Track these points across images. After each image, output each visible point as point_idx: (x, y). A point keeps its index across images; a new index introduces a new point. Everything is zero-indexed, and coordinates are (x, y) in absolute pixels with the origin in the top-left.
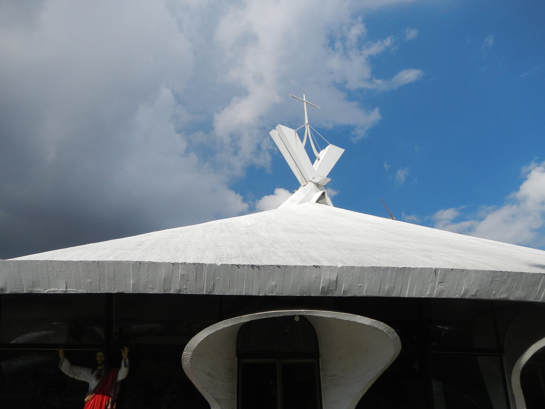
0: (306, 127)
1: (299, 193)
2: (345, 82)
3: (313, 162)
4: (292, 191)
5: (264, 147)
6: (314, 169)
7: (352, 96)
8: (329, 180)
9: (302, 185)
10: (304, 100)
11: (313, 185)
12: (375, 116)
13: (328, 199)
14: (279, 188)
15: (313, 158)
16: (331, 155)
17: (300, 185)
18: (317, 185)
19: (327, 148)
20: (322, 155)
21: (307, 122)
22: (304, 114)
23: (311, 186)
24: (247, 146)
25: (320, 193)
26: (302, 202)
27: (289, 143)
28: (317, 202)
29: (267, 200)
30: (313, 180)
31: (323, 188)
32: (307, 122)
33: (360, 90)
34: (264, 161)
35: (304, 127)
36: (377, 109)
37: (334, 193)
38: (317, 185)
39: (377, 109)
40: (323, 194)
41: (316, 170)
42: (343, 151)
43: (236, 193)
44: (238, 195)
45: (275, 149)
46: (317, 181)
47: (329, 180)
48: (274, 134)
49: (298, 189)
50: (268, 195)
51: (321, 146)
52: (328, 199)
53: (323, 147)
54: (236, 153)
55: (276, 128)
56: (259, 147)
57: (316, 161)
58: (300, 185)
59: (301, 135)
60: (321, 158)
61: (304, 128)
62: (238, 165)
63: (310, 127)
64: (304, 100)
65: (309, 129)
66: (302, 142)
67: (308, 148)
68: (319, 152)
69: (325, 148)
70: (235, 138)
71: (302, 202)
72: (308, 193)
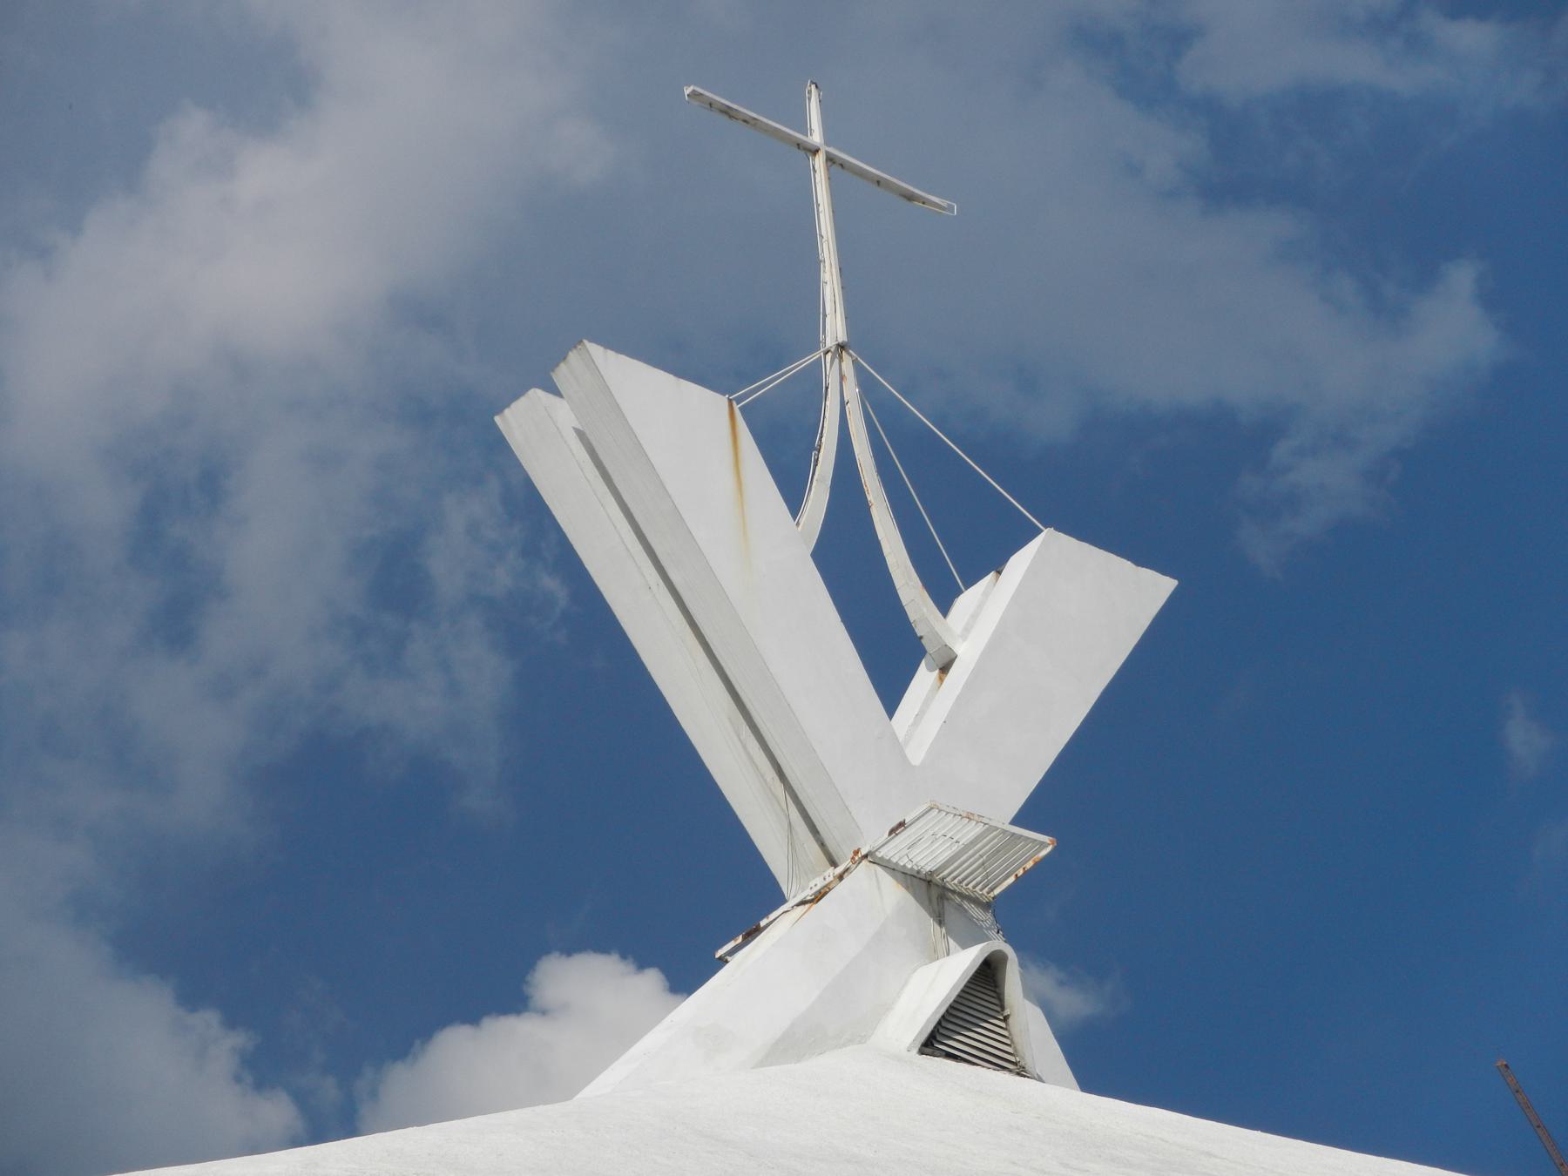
0: (832, 379)
1: (761, 976)
2: (1180, 39)
3: (891, 691)
4: (687, 970)
5: (448, 565)
6: (898, 747)
7: (1246, 161)
8: (1042, 845)
9: (794, 892)
10: (816, 138)
11: (894, 894)
12: (1453, 330)
13: (1028, 1022)
14: (570, 948)
15: (891, 656)
16: (1052, 626)
17: (768, 896)
18: (934, 893)
19: (1020, 562)
20: (977, 620)
21: (835, 328)
22: (816, 264)
23: (872, 899)
24: (280, 558)
25: (962, 962)
26: (792, 1045)
27: (675, 506)
28: (931, 1044)
29: (457, 1048)
30: (894, 851)
31: (986, 918)
32: (835, 328)
33: (1314, 107)
34: (449, 695)
35: (816, 369)
36: (1462, 277)
37: (1076, 1004)
38: (934, 893)
39: (1462, 277)
40: (988, 975)
41: (917, 754)
42: (1168, 585)
43: (190, 999)
44: (208, 1019)
45: (551, 584)
46: (926, 856)
47: (1042, 845)
48: (539, 430)
49: (752, 933)
50: (473, 1018)
51: (966, 549)
52: (1028, 1022)
53: (987, 557)
54: (175, 626)
55: (561, 375)
56: (393, 579)
57: (924, 677)
58: (768, 896)
59: (785, 449)
60: (967, 653)
61: (812, 389)
62: (199, 735)
63: (867, 386)
64: (816, 138)
65: (852, 391)
66: (794, 499)
67: (846, 561)
68: (944, 606)
69: (997, 564)
70: (176, 490)
71: (792, 1045)
72: (833, 989)
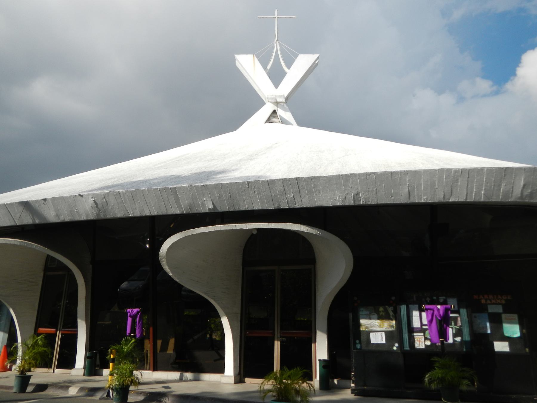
66: (264, 65)
